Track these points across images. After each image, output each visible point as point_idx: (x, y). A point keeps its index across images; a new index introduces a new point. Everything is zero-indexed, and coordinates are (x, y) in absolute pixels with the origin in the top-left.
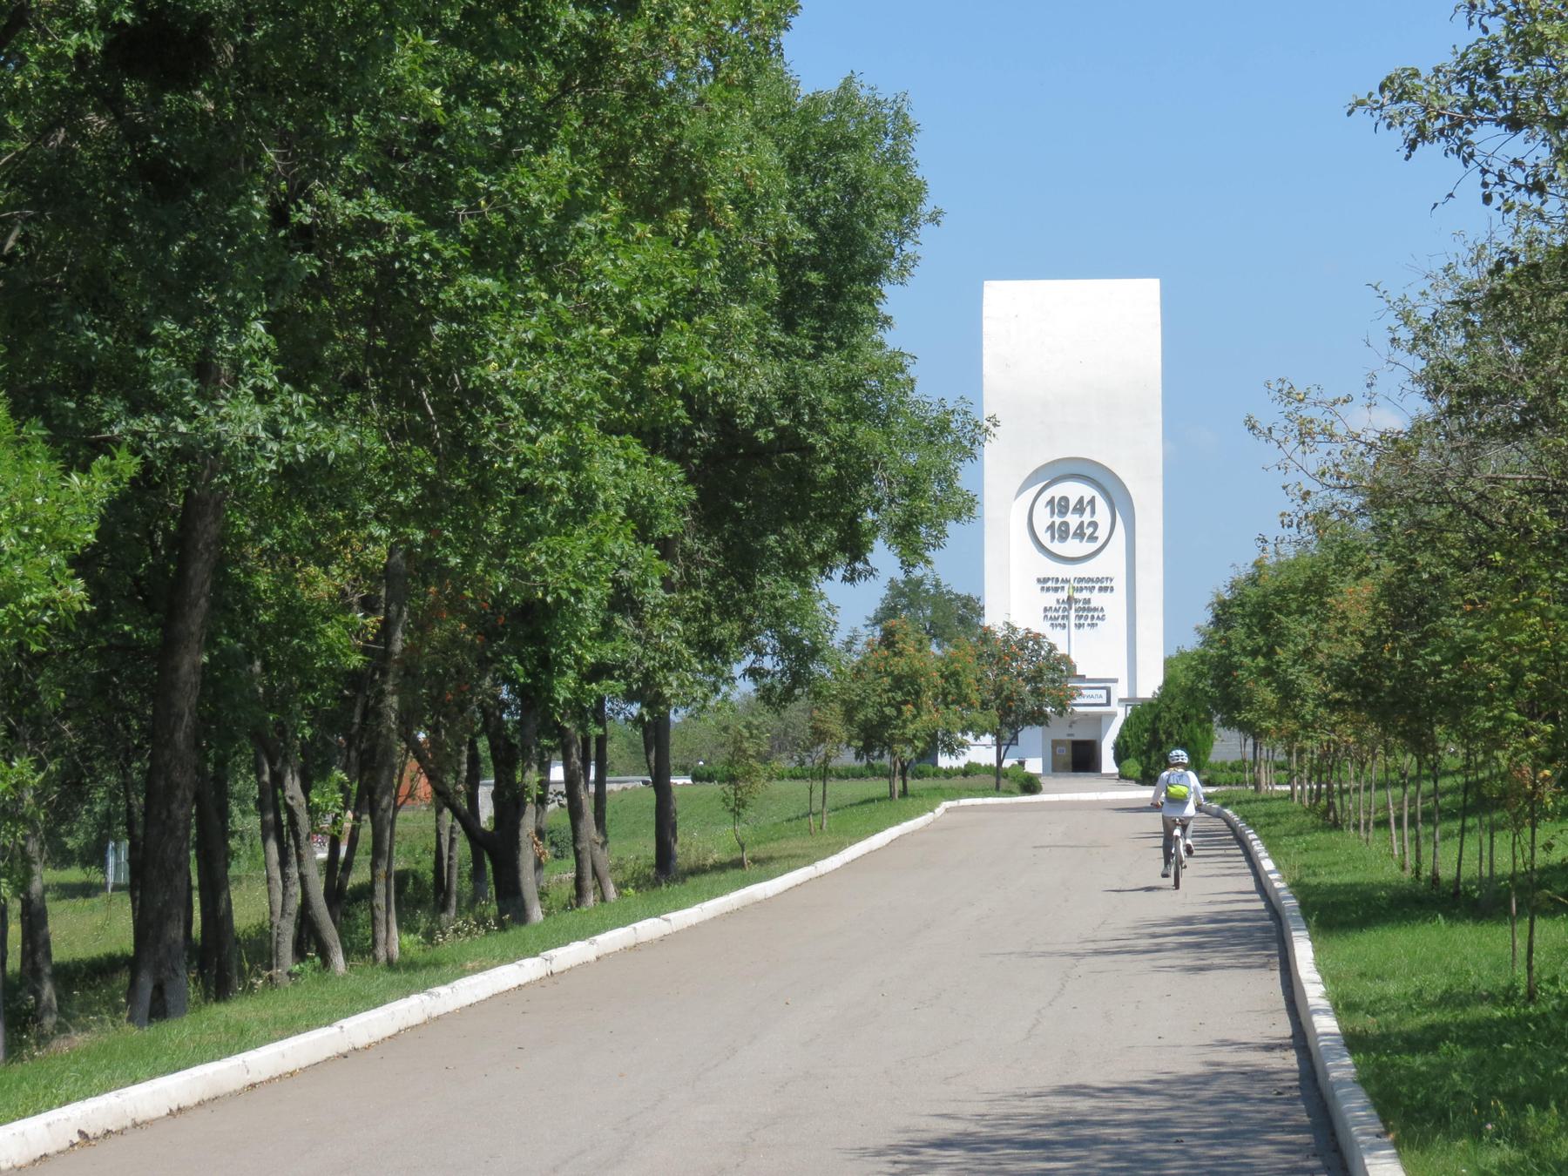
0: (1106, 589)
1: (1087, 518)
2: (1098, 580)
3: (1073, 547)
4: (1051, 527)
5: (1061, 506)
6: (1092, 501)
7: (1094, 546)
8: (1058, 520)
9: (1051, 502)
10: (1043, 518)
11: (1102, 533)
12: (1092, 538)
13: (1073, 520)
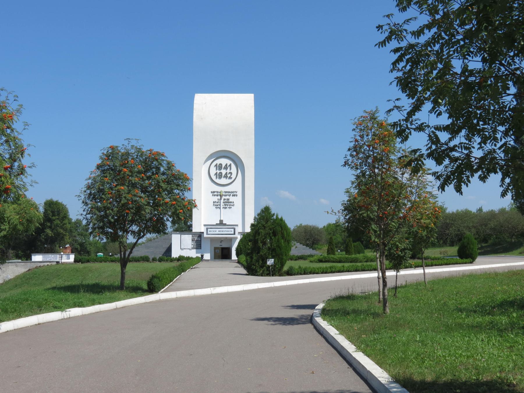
0: (235, 195)
1: (228, 171)
2: (232, 192)
3: (223, 181)
4: (216, 174)
5: (219, 167)
6: (230, 165)
7: (231, 181)
8: (218, 172)
9: (216, 165)
10: (213, 171)
11: (234, 176)
12: (230, 178)
13: (224, 172)
